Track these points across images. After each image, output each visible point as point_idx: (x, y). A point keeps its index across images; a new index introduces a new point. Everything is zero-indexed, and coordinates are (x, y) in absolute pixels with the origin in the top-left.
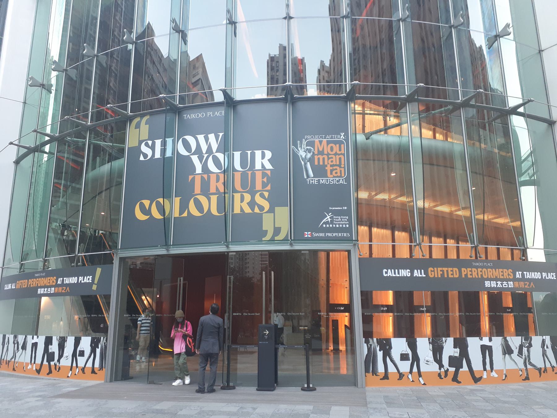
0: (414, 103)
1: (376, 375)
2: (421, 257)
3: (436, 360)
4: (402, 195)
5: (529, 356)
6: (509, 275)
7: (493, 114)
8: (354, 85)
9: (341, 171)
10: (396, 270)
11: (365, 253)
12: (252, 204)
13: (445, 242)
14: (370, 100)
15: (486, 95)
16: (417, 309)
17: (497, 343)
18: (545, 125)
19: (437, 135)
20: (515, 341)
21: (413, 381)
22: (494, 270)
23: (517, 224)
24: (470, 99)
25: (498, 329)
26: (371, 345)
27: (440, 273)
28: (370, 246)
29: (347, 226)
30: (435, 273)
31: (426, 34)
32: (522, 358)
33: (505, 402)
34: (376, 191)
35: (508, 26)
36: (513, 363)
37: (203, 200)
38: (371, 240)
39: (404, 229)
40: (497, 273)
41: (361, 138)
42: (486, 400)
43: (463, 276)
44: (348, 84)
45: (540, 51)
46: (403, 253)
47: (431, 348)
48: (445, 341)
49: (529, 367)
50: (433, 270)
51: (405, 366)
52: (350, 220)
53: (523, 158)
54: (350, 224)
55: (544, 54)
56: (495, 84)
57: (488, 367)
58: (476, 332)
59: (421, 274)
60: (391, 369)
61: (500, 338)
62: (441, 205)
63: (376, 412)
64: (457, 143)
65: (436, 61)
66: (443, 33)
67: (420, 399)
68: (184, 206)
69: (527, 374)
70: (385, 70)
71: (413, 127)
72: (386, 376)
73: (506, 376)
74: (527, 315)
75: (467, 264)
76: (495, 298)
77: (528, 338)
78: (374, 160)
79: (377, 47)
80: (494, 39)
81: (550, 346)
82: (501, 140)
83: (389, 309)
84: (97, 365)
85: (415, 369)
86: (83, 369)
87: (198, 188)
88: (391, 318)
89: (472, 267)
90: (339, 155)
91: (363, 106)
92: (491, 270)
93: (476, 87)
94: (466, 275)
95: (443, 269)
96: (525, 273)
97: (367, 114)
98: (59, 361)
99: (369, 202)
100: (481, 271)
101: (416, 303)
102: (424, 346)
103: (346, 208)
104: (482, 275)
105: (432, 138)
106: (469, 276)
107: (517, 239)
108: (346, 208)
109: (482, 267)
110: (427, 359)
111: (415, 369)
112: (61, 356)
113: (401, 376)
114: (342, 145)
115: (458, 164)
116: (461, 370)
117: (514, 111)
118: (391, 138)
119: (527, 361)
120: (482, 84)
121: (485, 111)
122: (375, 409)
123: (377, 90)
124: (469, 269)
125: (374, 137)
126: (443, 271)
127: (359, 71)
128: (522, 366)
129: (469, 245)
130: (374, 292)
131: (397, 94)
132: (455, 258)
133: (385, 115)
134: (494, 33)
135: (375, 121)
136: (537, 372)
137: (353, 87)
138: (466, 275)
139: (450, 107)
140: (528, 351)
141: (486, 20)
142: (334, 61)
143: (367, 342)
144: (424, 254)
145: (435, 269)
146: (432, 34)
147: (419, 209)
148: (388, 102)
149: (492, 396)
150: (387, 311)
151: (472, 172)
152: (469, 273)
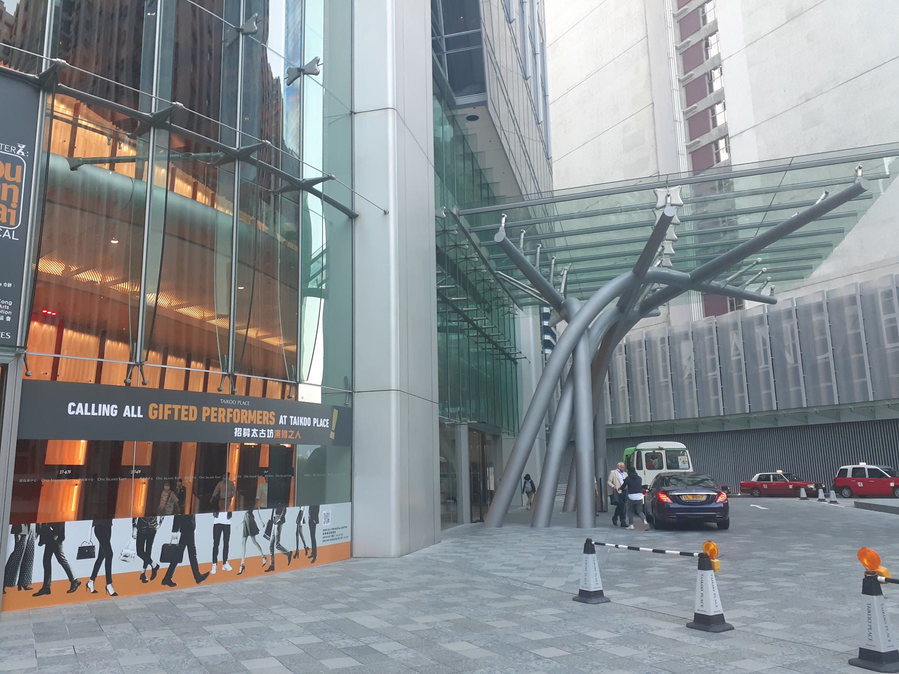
0: (163, 131)
1: (26, 589)
2: (140, 385)
3: (140, 553)
4: (124, 281)
5: (279, 536)
6: (269, 419)
7: (282, 184)
8: (57, 64)
9: (9, 215)
10: (93, 405)
11: (43, 372)
13: (188, 365)
14: (90, 104)
15: (277, 152)
16: (125, 472)
17: (238, 520)
18: (345, 217)
19: (199, 195)
20: (263, 516)
21: (95, 592)
22: (250, 411)
23: (293, 348)
24: (251, 150)
25: (248, 503)
26: (23, 536)
27: (167, 412)
28: (56, 361)
29: (8, 319)
30: (159, 412)
31: (201, 27)
32: (268, 539)
33: (234, 606)
34: (78, 265)
35: (316, 61)
36: (256, 547)
38: (58, 350)
39: (122, 337)
40: (254, 416)
41: (59, 164)
42: (208, 607)
43: (204, 419)
44: (46, 59)
45: (352, 113)
46: (116, 377)
47: (135, 533)
48: (161, 522)
49: (276, 551)
50: (156, 406)
51: (83, 569)
52: (15, 309)
53: (313, 257)
54: (15, 317)
55: (356, 117)
56: (290, 143)
57: (220, 557)
58: (214, 507)
59: (136, 413)
60: (58, 573)
61: (33, 376)
62: (188, 306)
63: (13, 654)
64: (226, 214)
65: (210, 77)
66: (227, 35)
67: (101, 620)
69: (273, 563)
70: (123, 61)
71: (156, 169)
72: (46, 589)
73: (243, 568)
75: (213, 400)
76: (249, 456)
77: (281, 512)
78: (83, 210)
79: (113, 16)
80: (297, 73)
81: (307, 521)
82: (289, 226)
83: (75, 472)
85: (102, 571)
88: (76, 487)
89: (219, 405)
90: (9, 183)
91: (76, 110)
92: (245, 411)
93: (262, 134)
94: (208, 418)
95: (174, 406)
96: (291, 417)
97: (81, 125)
99: (63, 283)
100: (232, 413)
101: (124, 462)
102: (123, 532)
103: (10, 285)
104: (231, 419)
105: (191, 197)
106: (213, 420)
107: (289, 370)
108: (10, 285)
109: (233, 407)
110: (125, 552)
111: (102, 571)
113: (74, 584)
114: (18, 168)
115: (221, 246)
116: (179, 565)
117: (309, 186)
118: (121, 178)
119: (276, 543)
120: (273, 136)
121: (273, 176)
122: (10, 649)
123: (106, 90)
124: (214, 409)
125: (85, 167)
126: (173, 410)
127: (75, 46)
128: (267, 552)
129: (219, 372)
131: (137, 108)
132: (201, 390)
133: (116, 140)
134: (298, 65)
135: (93, 141)
136: (286, 557)
137: (55, 67)
138: (208, 418)
139: (221, 154)
140: (279, 529)
141: (290, 42)
142: (26, 9)
143: (16, 531)
144: (146, 380)
145: (161, 405)
146: (210, 32)
147: (149, 307)
148: (121, 117)
149: (219, 600)
150: (69, 477)
151: (239, 261)
152: (214, 415)
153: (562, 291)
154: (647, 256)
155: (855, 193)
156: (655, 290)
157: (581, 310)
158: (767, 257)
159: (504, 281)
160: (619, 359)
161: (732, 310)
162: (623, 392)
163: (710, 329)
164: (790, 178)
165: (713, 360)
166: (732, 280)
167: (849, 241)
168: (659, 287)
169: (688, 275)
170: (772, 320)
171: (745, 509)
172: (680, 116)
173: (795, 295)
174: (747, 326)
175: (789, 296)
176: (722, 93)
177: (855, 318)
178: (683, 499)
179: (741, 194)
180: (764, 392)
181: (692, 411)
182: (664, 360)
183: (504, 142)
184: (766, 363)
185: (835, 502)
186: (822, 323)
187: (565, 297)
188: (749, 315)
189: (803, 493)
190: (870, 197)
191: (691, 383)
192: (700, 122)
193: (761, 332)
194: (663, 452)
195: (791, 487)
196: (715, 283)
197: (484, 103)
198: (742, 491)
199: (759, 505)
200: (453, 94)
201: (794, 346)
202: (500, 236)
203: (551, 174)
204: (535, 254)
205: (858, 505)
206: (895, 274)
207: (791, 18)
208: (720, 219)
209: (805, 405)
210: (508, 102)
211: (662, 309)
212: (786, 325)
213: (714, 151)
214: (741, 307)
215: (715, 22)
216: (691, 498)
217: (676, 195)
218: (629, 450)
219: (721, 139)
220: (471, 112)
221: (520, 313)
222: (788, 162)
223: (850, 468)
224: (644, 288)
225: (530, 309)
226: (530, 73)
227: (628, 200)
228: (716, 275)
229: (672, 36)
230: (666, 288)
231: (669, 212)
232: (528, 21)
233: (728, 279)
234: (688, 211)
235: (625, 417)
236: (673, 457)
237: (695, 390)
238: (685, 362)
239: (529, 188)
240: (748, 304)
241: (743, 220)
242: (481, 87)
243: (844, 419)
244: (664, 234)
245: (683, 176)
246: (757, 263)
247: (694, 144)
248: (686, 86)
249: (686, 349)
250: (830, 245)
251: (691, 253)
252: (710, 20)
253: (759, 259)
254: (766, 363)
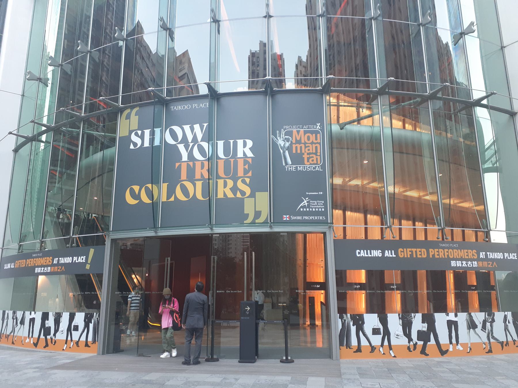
0: (385, 96)
1: (350, 348)
2: (391, 238)
3: (405, 334)
4: (373, 181)
5: (492, 330)
6: (473, 255)
7: (459, 106)
8: (329, 79)
9: (317, 159)
10: (369, 251)
11: (340, 235)
12: (234, 189)
13: (414, 225)
14: (345, 93)
15: (452, 88)
16: (388, 287)
17: (462, 318)
18: (507, 116)
19: (407, 125)
20: (479, 317)
21: (384, 354)
22: (459, 250)
23: (481, 208)
24: (437, 92)
25: (463, 305)
26: (345, 320)
27: (409, 253)
28: (345, 229)
29: (323, 210)
30: (404, 253)
31: (396, 32)
32: (485, 332)
33: (470, 373)
34: (349, 177)
35: (472, 24)
36: (477, 337)
37: (189, 185)
38: (345, 223)
39: (375, 213)
40: (462, 253)
41: (335, 128)
42: (452, 371)
43: (431, 256)
44: (324, 78)
45: (502, 48)
46: (375, 235)
47: (401, 323)
48: (414, 317)
49: (492, 340)
50: (402, 250)
51: (376, 340)
52: (325, 204)
53: (486, 147)
54: (326, 208)
55: (506, 50)
56: (460, 78)
57: (454, 341)
58: (443, 308)
59: (392, 254)
60: (364, 342)
62: (410, 190)
63: (350, 382)
64: (425, 133)
65: (405, 57)
66: (412, 30)
67: (390, 371)
68: (171, 192)
69: (491, 347)
70: (358, 65)
71: (384, 118)
72: (359, 349)
73: (470, 349)
75: (434, 245)
76: (460, 277)
77: (491, 314)
78: (348, 149)
79: (350, 44)
80: (459, 37)
81: (511, 321)
82: (466, 130)
83: (362, 287)
84: (90, 339)
85: (386, 343)
86: (77, 343)
87: (184, 175)
88: (364, 295)
89: (439, 248)
90: (315, 143)
91: (338, 98)
92: (456, 250)
93: (443, 81)
94: (433, 255)
95: (412, 249)
96: (488, 253)
97: (341, 106)
98: (55, 335)
99: (343, 188)
100: (448, 252)
101: (387, 281)
102: (394, 321)
103: (322, 193)
104: (448, 255)
105: (402, 128)
106: (436, 257)
107: (481, 222)
108: (322, 193)
109: (448, 248)
110: (397, 333)
111: (386, 343)
112: (56, 331)
113: (373, 349)
114: (318, 135)
115: (426, 152)
116: (429, 343)
117: (478, 103)
118: (364, 128)
119: (490, 335)
120: (448, 78)
121: (451, 103)
122: (348, 379)
123: (351, 84)
124: (436, 250)
125: (348, 127)
126: (412, 252)
127: (334, 66)
128: (485, 340)
129: (436, 227)
131: (369, 87)
132: (424, 239)
133: (358, 107)
134: (459, 31)
135: (348, 112)
136: (500, 345)
137: (329, 81)
138: (433, 255)
139: (419, 99)
140: (491, 326)
141: (452, 19)
142: (310, 56)
143: (341, 317)
144: (395, 236)
145: (405, 249)
146: (401, 32)
147: (390, 194)
148: (361, 94)
149: (458, 367)
150: (360, 289)
151: (439, 160)
152: (436, 253)
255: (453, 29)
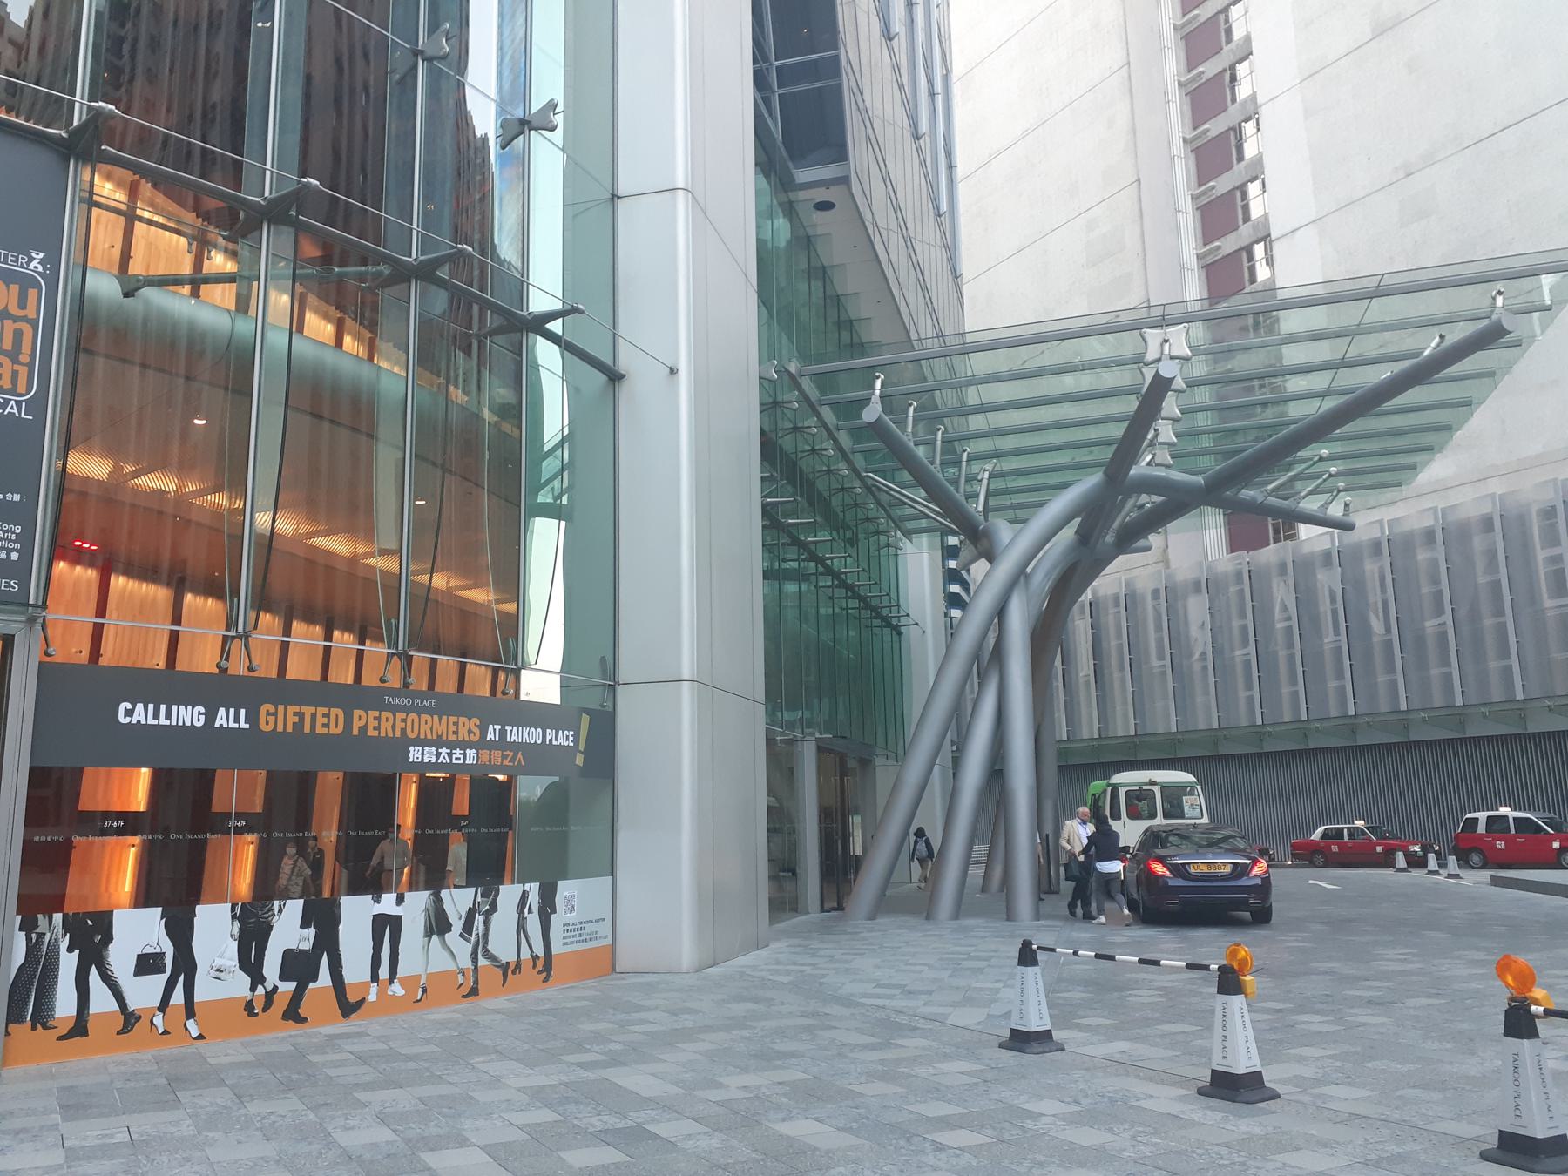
0: (285, 229)
1: (45, 1027)
2: (244, 672)
3: (245, 964)
4: (217, 489)
5: (486, 935)
6: (470, 732)
7: (493, 321)
8: (99, 111)
9: (15, 375)
10: (163, 707)
11: (75, 650)
13: (328, 637)
14: (158, 181)
15: (483, 266)
16: (219, 824)
17: (414, 908)
18: (602, 378)
19: (347, 339)
20: (458, 900)
21: (166, 1032)
22: (436, 717)
23: (510, 607)
24: (438, 263)
25: (433, 877)
26: (41, 936)
27: (292, 719)
28: (98, 630)
29: (15, 556)
30: (277, 719)
31: (351, 48)
32: (468, 941)
33: (409, 1058)
34: (136, 463)
35: (552, 106)
36: (446, 954)
38: (101, 611)
39: (212, 588)
40: (442, 726)
41: (103, 285)
42: (362, 1059)
43: (355, 732)
44: (81, 103)
45: (614, 197)
46: (202, 657)
47: (236, 931)
48: (280, 911)
49: (482, 962)
50: (272, 709)
51: (144, 992)
52: (26, 540)
53: (546, 449)
54: (27, 553)
55: (621, 204)
56: (506, 249)
57: (384, 972)
58: (373, 884)
59: (237, 720)
60: (101, 1000)
62: (328, 533)
63: (22, 1141)
64: (393, 374)
65: (366, 135)
66: (395, 60)
67: (175, 1082)
69: (476, 982)
70: (214, 106)
71: (273, 295)
72: (80, 1027)
73: (425, 991)
74: (205, 841)
75: (372, 699)
76: (434, 795)
77: (491, 893)
78: (144, 366)
79: (196, 28)
80: (518, 127)
81: (535, 908)
82: (503, 394)
83: (131, 823)
85: (178, 997)
88: (133, 850)
89: (382, 707)
90: (16, 319)
91: (133, 192)
92: (428, 717)
93: (457, 234)
94: (363, 729)
95: (304, 709)
96: (508, 728)
97: (141, 219)
99: (109, 494)
100: (404, 720)
101: (217, 807)
102: (214, 929)
103: (17, 497)
104: (404, 731)
105: (332, 343)
106: (371, 732)
107: (503, 645)
108: (17, 497)
109: (407, 710)
110: (219, 962)
111: (178, 997)
113: (130, 1019)
114: (32, 293)
115: (386, 429)
116: (312, 985)
117: (538, 324)
118: (212, 311)
119: (481, 948)
120: (477, 236)
121: (476, 308)
122: (17, 1133)
123: (184, 158)
124: (373, 713)
125: (148, 292)
126: (301, 715)
127: (131, 80)
128: (466, 963)
129: (382, 649)
130: (320, 774)
131: (238, 188)
132: (350, 680)
133: (201, 245)
134: (519, 113)
135: (163, 246)
136: (499, 972)
137: (95, 117)
138: (363, 729)
139: (385, 269)
140: (487, 923)
141: (506, 73)
142: (46, 15)
143: (28, 926)
144: (255, 663)
145: (281, 707)
146: (366, 56)
147: (260, 536)
148: (211, 204)
149: (381, 1046)
150: (121, 832)
151: (417, 456)
152: (372, 723)
153: (980, 508)
154: (1129, 447)
155: (1492, 336)
156: (1142, 506)
157: (1014, 541)
158: (1338, 448)
159: (880, 490)
160: (1080, 627)
161: (1277, 540)
162: (1087, 683)
163: (1239, 575)
164: (1378, 310)
165: (1244, 628)
166: (1276, 489)
167: (1480, 420)
168: (1149, 500)
169: (1200, 479)
170: (1347, 559)
171: (1299, 887)
172: (1185, 202)
173: (1387, 514)
174: (1303, 569)
175: (1375, 516)
176: (1258, 161)
177: (1491, 555)
178: (1192, 870)
179: (1292, 339)
180: (1332, 684)
181: (1206, 716)
182: (1159, 628)
183: (879, 247)
184: (1337, 633)
185: (1457, 876)
186: (1434, 563)
187: (986, 519)
188: (1306, 549)
189: (1401, 860)
190: (1517, 344)
191: (1205, 668)
192: (1220, 213)
193: (1328, 580)
194: (1157, 789)
195: (1379, 849)
196: (1246, 494)
197: (845, 180)
198: (1295, 856)
199: (1324, 881)
200: (790, 164)
201: (1385, 603)
202: (873, 412)
203: (962, 304)
204: (933, 443)
205: (1496, 881)
206: (1561, 477)
207: (1380, 31)
208: (1256, 383)
209: (1403, 707)
210: (886, 178)
211: (1154, 539)
212: (1370, 567)
213: (1246, 264)
214: (1292, 536)
215: (1248, 39)
216: (1205, 869)
217: (1179, 340)
218: (1097, 786)
219: (1258, 242)
220: (821, 195)
221: (907, 546)
222: (1374, 282)
223: (1482, 816)
224: (1124, 502)
225: (924, 539)
226: (924, 127)
227: (1096, 348)
228: (1248, 480)
229: (1172, 62)
230: (1162, 503)
231: (1167, 369)
232: (920, 37)
233: (1270, 487)
234: (1200, 369)
235: (1089, 728)
236: (1173, 797)
237: (1212, 680)
238: (1194, 631)
239: (923, 328)
240: (1305, 531)
241: (1296, 384)
242: (839, 153)
243: (1472, 732)
244: (1159, 409)
245: (1192, 307)
246: (1321, 459)
247: (1210, 252)
248: (1196, 151)
249: (1197, 610)
250: (1447, 428)
251: (1206, 442)
252: (1238, 34)
253: (1325, 452)
254: (1337, 633)
255: (502, 105)
